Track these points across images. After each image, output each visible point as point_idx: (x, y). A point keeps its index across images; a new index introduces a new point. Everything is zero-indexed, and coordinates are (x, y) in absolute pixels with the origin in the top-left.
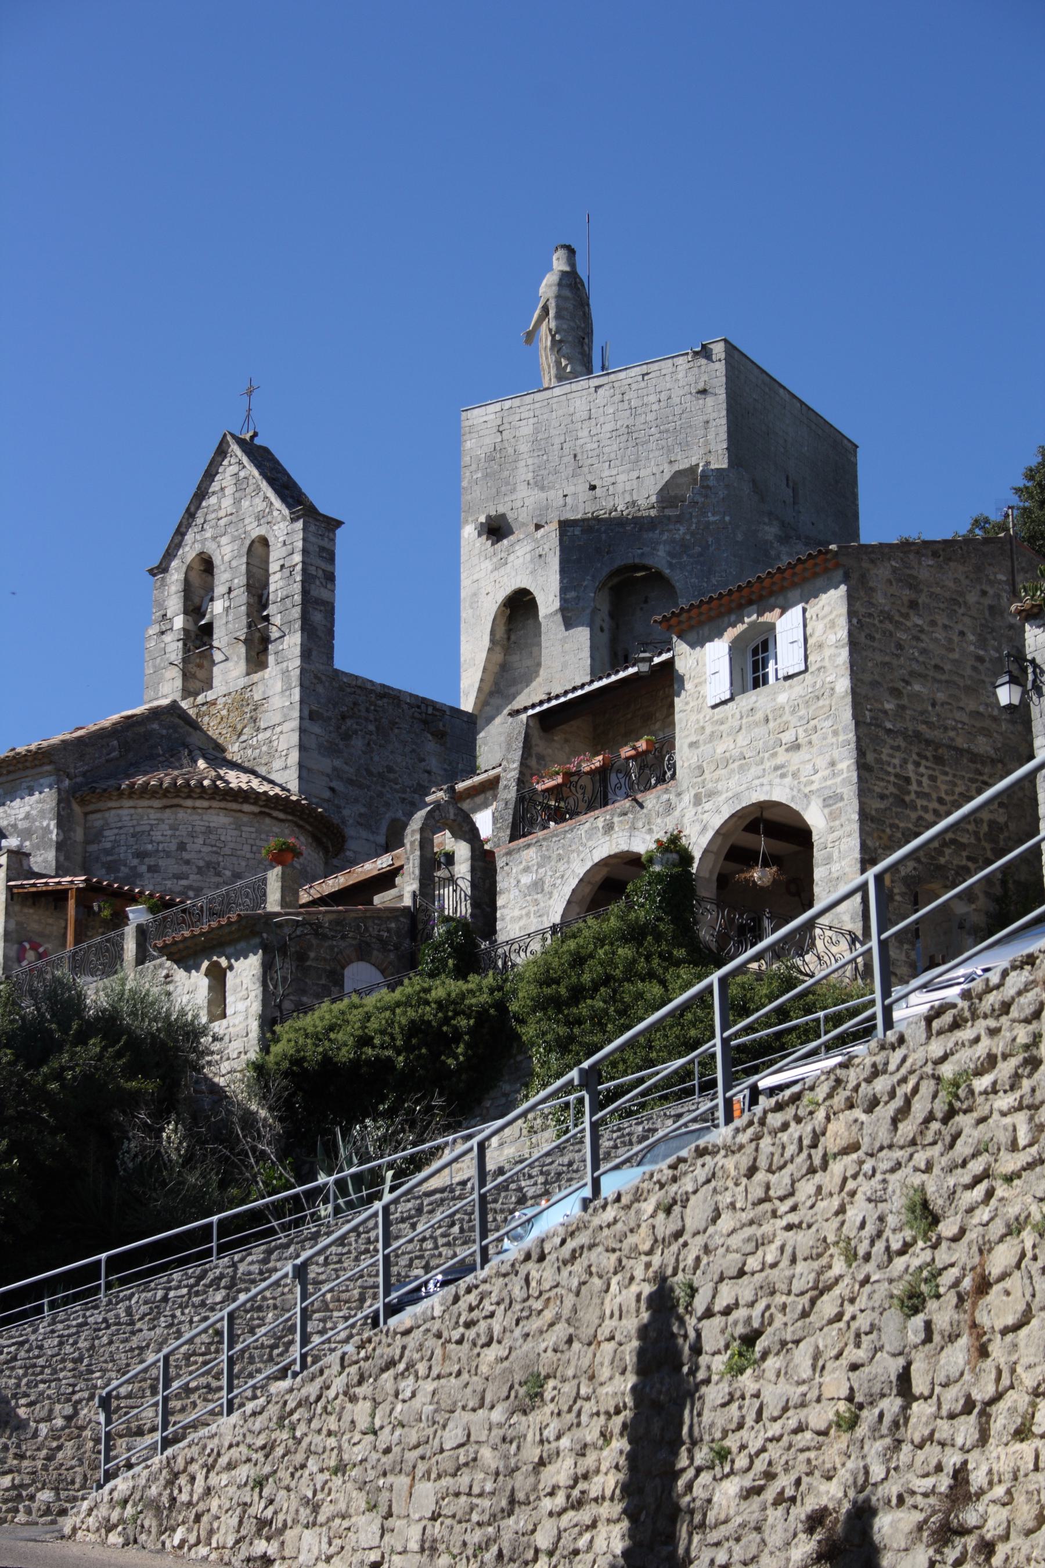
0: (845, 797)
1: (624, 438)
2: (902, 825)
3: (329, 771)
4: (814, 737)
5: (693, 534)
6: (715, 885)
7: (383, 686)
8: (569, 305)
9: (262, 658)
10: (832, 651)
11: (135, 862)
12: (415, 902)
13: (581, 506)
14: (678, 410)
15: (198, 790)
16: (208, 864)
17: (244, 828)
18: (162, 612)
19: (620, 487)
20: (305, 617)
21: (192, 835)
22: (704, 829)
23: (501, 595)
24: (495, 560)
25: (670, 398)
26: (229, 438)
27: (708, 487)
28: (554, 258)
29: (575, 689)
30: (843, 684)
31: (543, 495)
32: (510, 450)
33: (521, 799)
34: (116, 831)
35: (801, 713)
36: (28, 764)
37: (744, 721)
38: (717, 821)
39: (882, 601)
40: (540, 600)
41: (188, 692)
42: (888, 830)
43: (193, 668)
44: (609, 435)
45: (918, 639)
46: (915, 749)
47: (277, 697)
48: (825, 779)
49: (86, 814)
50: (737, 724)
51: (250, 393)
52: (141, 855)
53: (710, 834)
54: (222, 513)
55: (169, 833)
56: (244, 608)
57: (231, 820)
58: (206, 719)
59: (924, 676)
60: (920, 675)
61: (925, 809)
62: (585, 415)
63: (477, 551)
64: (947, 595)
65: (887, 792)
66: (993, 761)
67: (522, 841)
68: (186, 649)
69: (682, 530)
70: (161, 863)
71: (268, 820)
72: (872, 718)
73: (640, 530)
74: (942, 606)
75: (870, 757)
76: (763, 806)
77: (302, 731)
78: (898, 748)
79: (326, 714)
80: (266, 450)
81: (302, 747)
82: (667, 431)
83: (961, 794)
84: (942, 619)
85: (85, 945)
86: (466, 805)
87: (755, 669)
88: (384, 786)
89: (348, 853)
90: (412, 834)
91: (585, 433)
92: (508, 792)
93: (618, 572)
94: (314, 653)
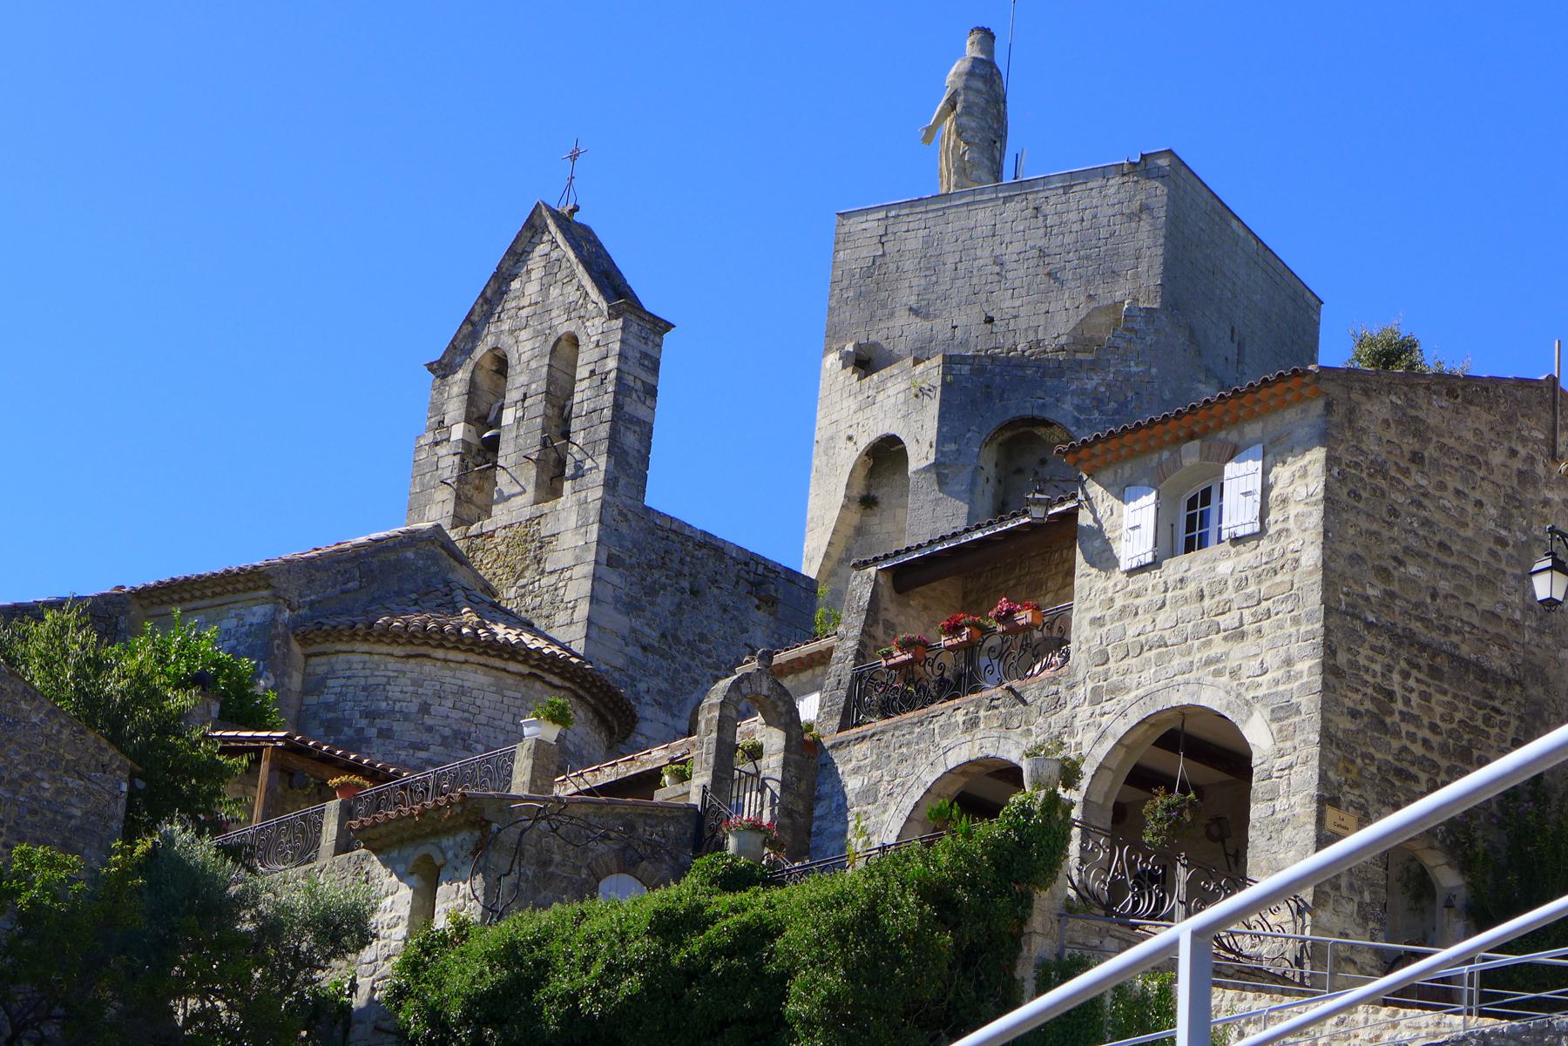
0: (1303, 709)
1: (1032, 263)
2: (1378, 756)
3: (626, 632)
4: (1265, 623)
5: (1109, 386)
6: (1109, 815)
7: (705, 533)
8: (980, 101)
9: (556, 483)
10: (1301, 508)
11: (363, 723)
12: (704, 799)
13: (973, 340)
14: (1104, 233)
15: (453, 639)
16: (456, 733)
17: (507, 693)
18: (438, 418)
19: (1022, 323)
20: (613, 437)
21: (439, 696)
22: (1102, 736)
23: (864, 441)
24: (860, 398)
25: (1095, 217)
26: (545, 213)
27: (1132, 330)
28: (968, 43)
29: (943, 538)
30: (1311, 556)
31: (928, 324)
32: (892, 267)
33: (858, 677)
34: (343, 681)
35: (1248, 591)
36: (240, 586)
37: (1169, 595)
38: (1121, 728)
39: (1375, 448)
40: (911, 450)
41: (459, 520)
42: (1359, 761)
43: (469, 490)
44: (1015, 257)
45: (1420, 505)
46: (1404, 654)
47: (569, 534)
48: (1277, 682)
49: (308, 656)
50: (1159, 597)
51: (574, 157)
52: (371, 715)
53: (1109, 744)
54: (525, 302)
55: (411, 689)
56: (539, 420)
57: (491, 680)
58: (479, 554)
59: (1425, 556)
60: (1420, 555)
61: (1412, 737)
62: (987, 231)
63: (839, 386)
64: (1464, 449)
65: (1361, 709)
66: (1509, 681)
67: (853, 732)
68: (464, 467)
69: (1096, 379)
70: (396, 726)
71: (538, 685)
72: (1347, 605)
73: (1043, 375)
74: (1455, 463)
75: (1342, 658)
76: (1184, 712)
77: (596, 578)
78: (1380, 650)
79: (628, 561)
80: (587, 230)
81: (594, 599)
82: (1088, 257)
83: (1461, 721)
84: (1453, 483)
85: (274, 821)
86: (788, 682)
87: (1190, 526)
88: (693, 659)
89: (639, 738)
90: (708, 716)
91: (987, 252)
92: (843, 666)
93: (1012, 424)
94: (622, 482)
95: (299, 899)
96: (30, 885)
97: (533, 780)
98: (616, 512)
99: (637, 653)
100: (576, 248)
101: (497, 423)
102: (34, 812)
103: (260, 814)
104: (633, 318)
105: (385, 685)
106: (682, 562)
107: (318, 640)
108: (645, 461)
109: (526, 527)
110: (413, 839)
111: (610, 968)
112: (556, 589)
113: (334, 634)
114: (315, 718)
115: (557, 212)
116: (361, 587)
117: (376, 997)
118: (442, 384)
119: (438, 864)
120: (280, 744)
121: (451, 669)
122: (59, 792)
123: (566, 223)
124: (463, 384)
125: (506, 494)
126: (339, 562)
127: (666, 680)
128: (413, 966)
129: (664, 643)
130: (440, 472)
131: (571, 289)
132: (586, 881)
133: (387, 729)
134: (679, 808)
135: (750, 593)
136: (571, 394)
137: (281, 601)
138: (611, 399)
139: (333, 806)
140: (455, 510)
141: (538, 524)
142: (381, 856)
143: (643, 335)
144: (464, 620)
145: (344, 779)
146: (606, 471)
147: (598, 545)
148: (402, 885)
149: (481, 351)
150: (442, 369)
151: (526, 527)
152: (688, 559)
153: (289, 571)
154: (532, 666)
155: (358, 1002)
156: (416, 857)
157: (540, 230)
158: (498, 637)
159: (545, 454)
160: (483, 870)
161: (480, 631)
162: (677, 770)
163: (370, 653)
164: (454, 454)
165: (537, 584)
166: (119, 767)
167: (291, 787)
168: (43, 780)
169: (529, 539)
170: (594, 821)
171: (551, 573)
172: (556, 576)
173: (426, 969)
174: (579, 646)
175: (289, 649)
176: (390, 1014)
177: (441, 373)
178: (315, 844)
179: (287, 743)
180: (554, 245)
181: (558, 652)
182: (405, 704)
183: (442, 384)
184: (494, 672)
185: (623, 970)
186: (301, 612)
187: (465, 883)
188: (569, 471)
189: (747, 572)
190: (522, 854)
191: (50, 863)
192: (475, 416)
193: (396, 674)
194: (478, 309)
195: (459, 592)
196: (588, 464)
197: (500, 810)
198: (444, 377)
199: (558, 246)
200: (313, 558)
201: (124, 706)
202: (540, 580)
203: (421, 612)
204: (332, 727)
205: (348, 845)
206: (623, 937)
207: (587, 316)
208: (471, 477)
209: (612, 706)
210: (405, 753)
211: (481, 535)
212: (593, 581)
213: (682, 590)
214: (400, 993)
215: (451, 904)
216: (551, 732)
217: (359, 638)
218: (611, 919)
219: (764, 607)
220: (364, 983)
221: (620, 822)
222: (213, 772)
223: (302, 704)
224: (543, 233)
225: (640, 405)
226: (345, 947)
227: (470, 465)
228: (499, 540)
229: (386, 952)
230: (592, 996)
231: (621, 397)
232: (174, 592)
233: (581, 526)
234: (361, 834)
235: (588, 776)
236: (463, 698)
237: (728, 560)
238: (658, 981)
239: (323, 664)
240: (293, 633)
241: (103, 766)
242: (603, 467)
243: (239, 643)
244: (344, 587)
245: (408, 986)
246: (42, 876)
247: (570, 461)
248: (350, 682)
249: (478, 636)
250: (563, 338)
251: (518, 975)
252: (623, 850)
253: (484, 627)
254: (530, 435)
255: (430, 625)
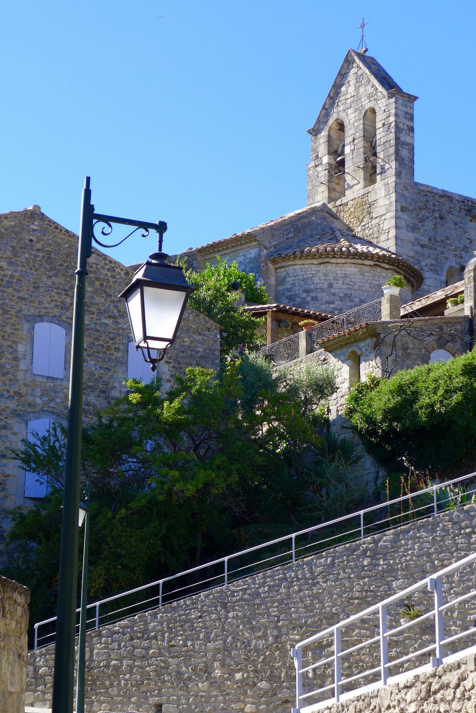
3: (413, 240)
7: (443, 191)
11: (304, 295)
12: (472, 312)
15: (339, 253)
16: (346, 295)
17: (365, 274)
20: (397, 153)
26: (353, 54)
34: (293, 278)
36: (243, 242)
41: (331, 200)
43: (333, 185)
47: (382, 199)
49: (276, 269)
51: (363, 26)
52: (307, 291)
54: (349, 96)
55: (323, 278)
56: (362, 149)
57: (358, 269)
58: (342, 213)
68: (330, 176)
70: (319, 295)
71: (379, 269)
77: (397, 218)
79: (410, 208)
80: (373, 59)
81: (397, 227)
89: (425, 287)
94: (403, 172)
95: (304, 377)
96: (195, 384)
97: (391, 313)
98: (402, 187)
99: (417, 248)
100: (369, 68)
101: (343, 153)
102: (183, 352)
103: (270, 340)
104: (399, 96)
105: (312, 278)
106: (434, 205)
107: (280, 261)
108: (412, 161)
109: (362, 199)
110: (346, 345)
111: (446, 391)
112: (379, 225)
113: (284, 259)
114: (283, 296)
115: (358, 53)
116: (295, 236)
117: (339, 413)
118: (315, 139)
119: (359, 354)
120: (274, 309)
121: (340, 267)
122: (192, 342)
123: (362, 57)
124: (325, 137)
125: (351, 185)
126: (284, 226)
127: (433, 259)
128: (356, 399)
129: (431, 243)
130: (319, 179)
131: (369, 87)
132: (424, 355)
133: (315, 297)
134: (461, 318)
135: (466, 215)
136: (375, 135)
137: (262, 246)
138: (394, 135)
139: (302, 334)
140: (329, 195)
141: (367, 196)
142: (333, 354)
143: (405, 104)
144: (342, 244)
145: (306, 321)
146: (395, 168)
147: (396, 202)
148: (344, 364)
149: (331, 121)
150: (315, 132)
151: (362, 199)
152: (437, 203)
153: (263, 233)
154: (375, 261)
155: (332, 417)
156: (349, 352)
157: (352, 62)
158: (359, 250)
159: (367, 164)
160: (380, 355)
161: (350, 249)
162: (453, 300)
163: (303, 264)
164: (325, 170)
165: (370, 224)
166: (215, 329)
167: (280, 327)
168: (184, 338)
169: (364, 204)
170: (425, 328)
171: (376, 218)
172: (378, 219)
173: (362, 400)
174: (393, 249)
175: (268, 267)
176: (347, 420)
177: (314, 134)
178: (297, 350)
179: (278, 309)
180: (359, 68)
181: (386, 253)
182: (321, 285)
183: (315, 139)
184: (359, 266)
185: (452, 392)
186: (271, 250)
187: (372, 361)
188: (378, 171)
189: (464, 206)
190: (396, 347)
191: (202, 374)
192: (332, 151)
193: (316, 272)
194: (328, 102)
195: (338, 232)
196: (387, 166)
197: (383, 328)
198: (316, 135)
199: (361, 68)
200: (273, 225)
201: (211, 302)
202: (371, 222)
203: (322, 243)
204: (291, 299)
205: (311, 349)
206: (450, 377)
207: (378, 99)
208: (333, 179)
209: (412, 274)
210: (324, 306)
211: (342, 205)
212: (396, 219)
213: (436, 218)
214: (351, 411)
215: (367, 371)
216: (396, 291)
217: (298, 258)
218: (443, 370)
219: (473, 220)
220: (333, 409)
221: (436, 327)
222: (251, 325)
223: (276, 290)
224: (353, 63)
225: (407, 136)
226: (326, 394)
227: (333, 173)
228: (350, 206)
229: (341, 394)
230: (440, 404)
231: (398, 134)
232: (215, 248)
233: (387, 195)
234: (323, 345)
235: (408, 308)
236: (347, 279)
237: (454, 201)
238: (469, 395)
239: (283, 272)
240: (269, 259)
241: (208, 329)
242: (394, 167)
243: (246, 267)
244: (287, 237)
245: (354, 408)
246: (200, 380)
247: (378, 166)
248: (296, 278)
249: (349, 250)
250: (368, 110)
251: (405, 398)
252: (439, 339)
253: (352, 247)
254: (358, 157)
255: (328, 249)
